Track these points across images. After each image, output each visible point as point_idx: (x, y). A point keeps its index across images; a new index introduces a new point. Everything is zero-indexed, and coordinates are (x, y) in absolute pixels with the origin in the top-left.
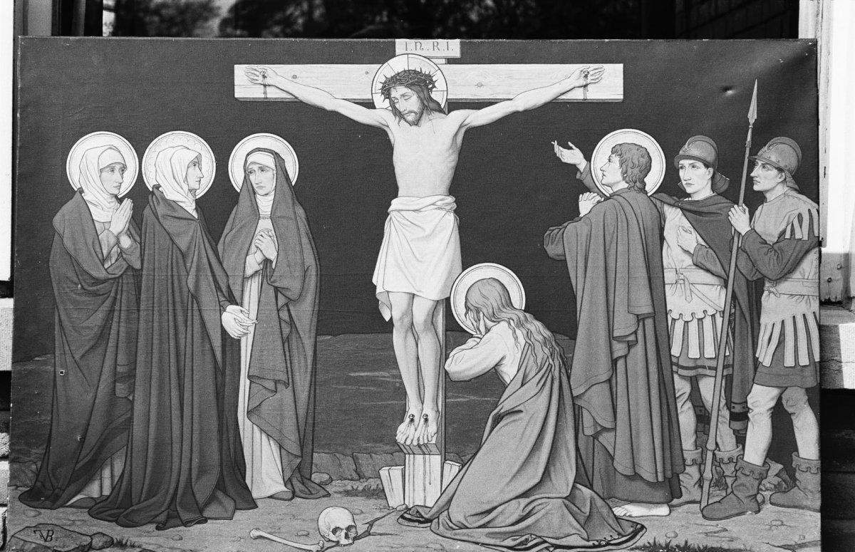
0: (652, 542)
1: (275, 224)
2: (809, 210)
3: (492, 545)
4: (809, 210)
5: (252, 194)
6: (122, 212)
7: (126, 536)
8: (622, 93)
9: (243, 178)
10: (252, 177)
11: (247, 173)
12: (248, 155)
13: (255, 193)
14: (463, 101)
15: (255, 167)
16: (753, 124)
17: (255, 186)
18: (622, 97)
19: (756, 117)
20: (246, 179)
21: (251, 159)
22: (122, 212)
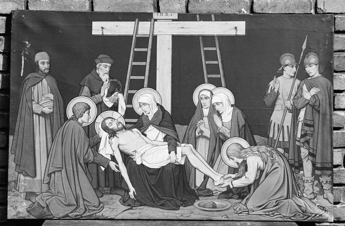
0: (117, 135)
1: (233, 114)
2: (272, 87)
3: (62, 139)
4: (272, 87)
5: (201, 107)
6: (217, 121)
7: (141, 151)
8: (93, 30)
9: (198, 102)
10: (202, 101)
11: (200, 99)
12: (200, 92)
13: (202, 107)
14: (136, 40)
15: (203, 97)
16: (304, 50)
17: (203, 105)
18: (245, 34)
19: (305, 48)
20: (199, 102)
21: (201, 93)
22: (217, 121)
